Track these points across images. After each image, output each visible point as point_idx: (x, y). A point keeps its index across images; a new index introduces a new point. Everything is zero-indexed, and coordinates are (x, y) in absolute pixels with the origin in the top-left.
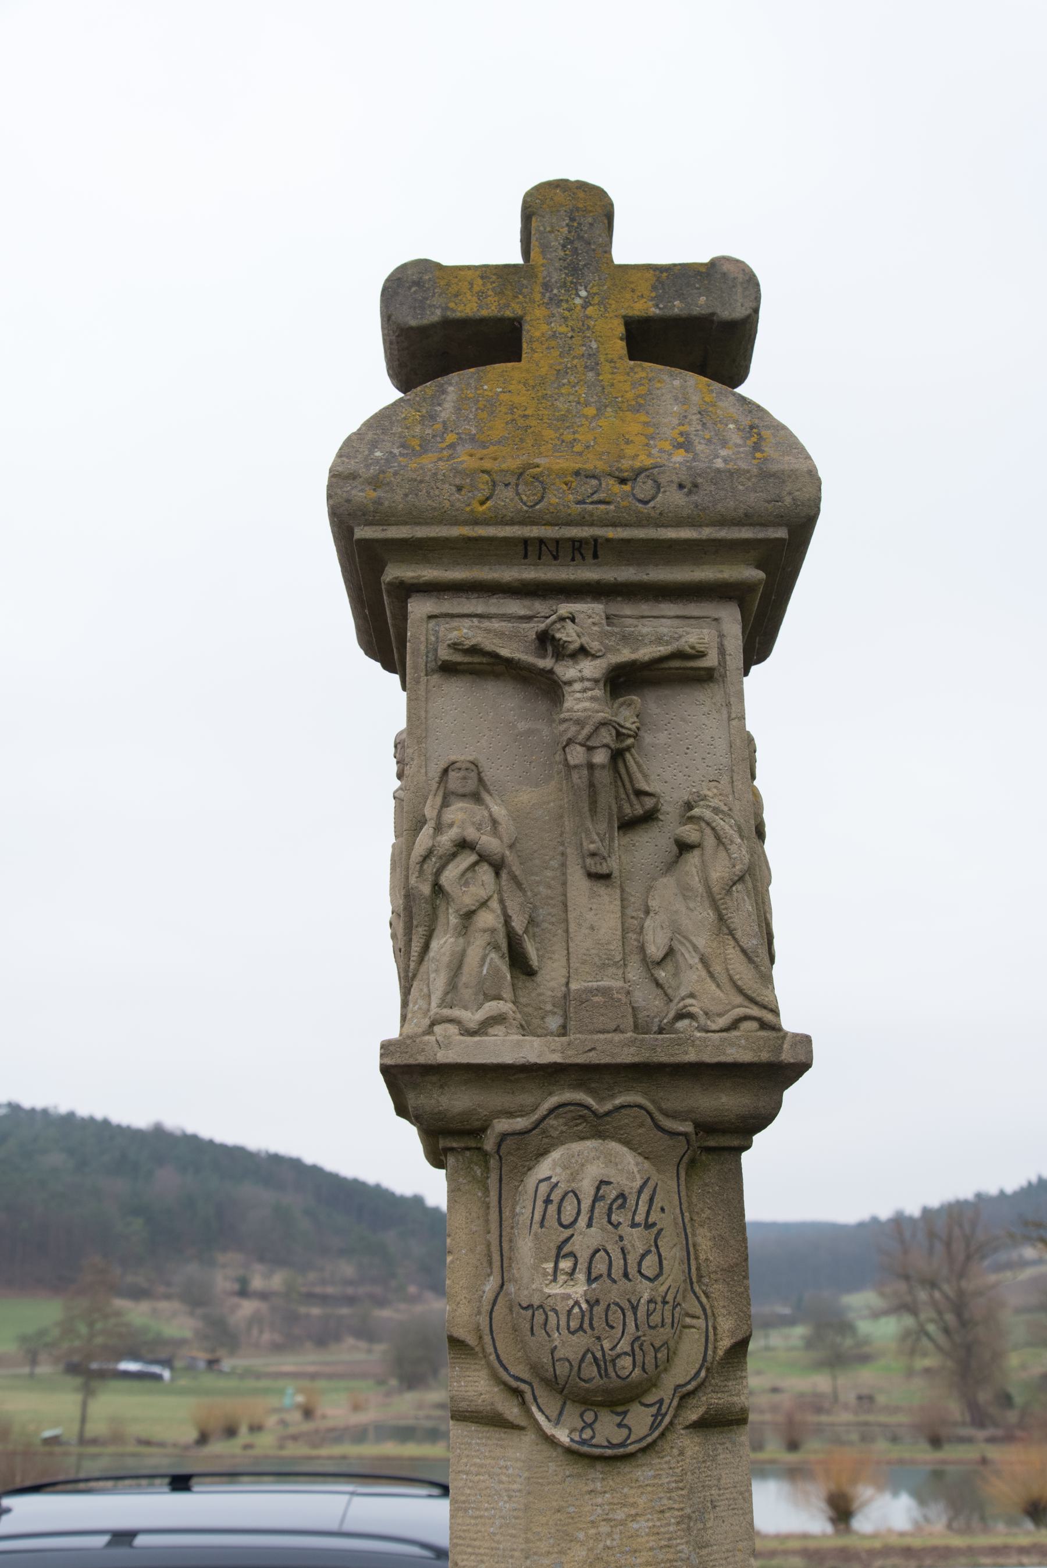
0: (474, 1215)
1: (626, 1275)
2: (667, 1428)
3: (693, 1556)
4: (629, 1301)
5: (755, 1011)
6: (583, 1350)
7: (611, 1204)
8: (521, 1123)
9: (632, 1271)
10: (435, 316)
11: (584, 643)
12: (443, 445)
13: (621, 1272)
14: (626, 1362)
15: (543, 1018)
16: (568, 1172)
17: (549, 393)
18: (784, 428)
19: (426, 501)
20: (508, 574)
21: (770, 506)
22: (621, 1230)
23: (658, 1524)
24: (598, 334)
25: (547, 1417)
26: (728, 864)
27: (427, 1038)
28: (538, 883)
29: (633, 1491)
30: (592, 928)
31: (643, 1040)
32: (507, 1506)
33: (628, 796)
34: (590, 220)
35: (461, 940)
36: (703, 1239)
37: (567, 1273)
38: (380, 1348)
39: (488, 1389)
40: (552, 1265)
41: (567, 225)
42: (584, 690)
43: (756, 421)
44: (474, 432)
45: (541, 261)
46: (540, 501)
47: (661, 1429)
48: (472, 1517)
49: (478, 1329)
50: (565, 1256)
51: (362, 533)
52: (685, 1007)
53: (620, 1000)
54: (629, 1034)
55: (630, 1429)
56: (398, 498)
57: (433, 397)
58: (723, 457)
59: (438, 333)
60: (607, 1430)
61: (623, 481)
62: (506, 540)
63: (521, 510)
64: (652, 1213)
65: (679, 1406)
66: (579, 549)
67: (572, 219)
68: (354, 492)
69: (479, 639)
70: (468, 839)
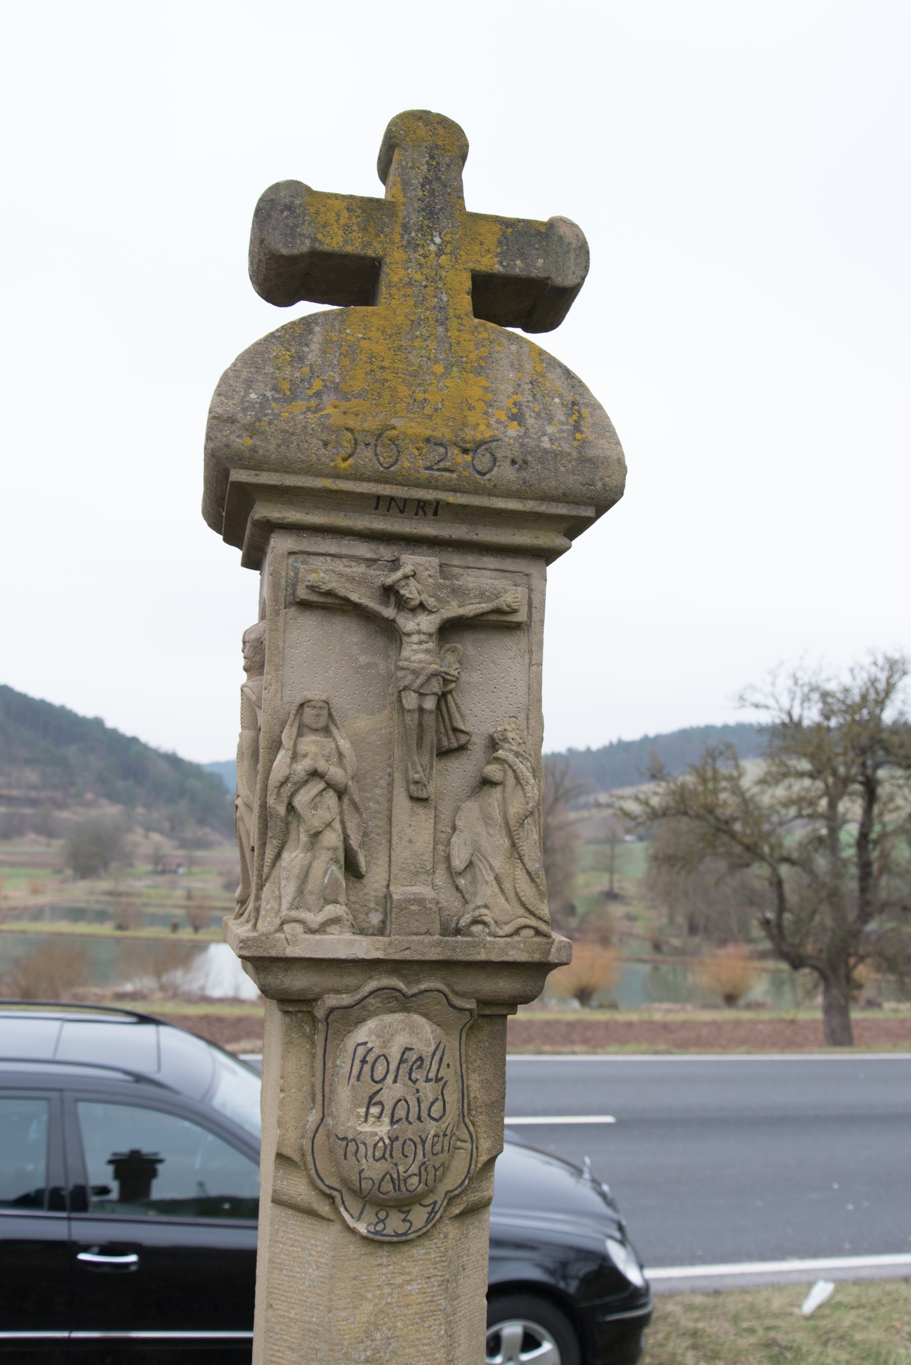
0: (303, 1062)
1: (419, 1118)
2: (438, 1220)
3: (449, 1306)
4: (420, 1137)
5: (533, 922)
6: (384, 1173)
7: (412, 1065)
8: (346, 999)
9: (424, 1115)
10: (304, 247)
11: (423, 600)
12: (310, 392)
13: (416, 1116)
14: (415, 1180)
15: (367, 914)
16: (381, 1040)
17: (404, 344)
18: (600, 407)
19: (296, 453)
20: (361, 522)
21: (584, 489)
22: (418, 1085)
23: (425, 1286)
24: (449, 286)
25: (351, 1215)
26: (523, 802)
27: (278, 935)
28: (369, 799)
29: (409, 1264)
30: (411, 842)
31: (447, 942)
32: (316, 1273)
33: (446, 731)
34: (447, 160)
35: (309, 855)
36: (474, 1083)
37: (375, 1117)
38: (58, 844)
39: (307, 1192)
40: (364, 1110)
41: (427, 163)
42: (421, 643)
43: (578, 397)
44: (337, 380)
45: (403, 200)
46: (395, 463)
47: (433, 1222)
48: (285, 1275)
49: (301, 1148)
50: (375, 1104)
51: (238, 475)
52: (481, 915)
53: (431, 909)
54: (437, 937)
55: (411, 1223)
56: (272, 448)
57: (301, 335)
58: (549, 435)
59: (305, 255)
60: (395, 1223)
61: (465, 451)
62: (362, 495)
63: (377, 471)
64: (441, 1070)
65: (448, 1204)
66: (423, 508)
67: (432, 157)
68: (232, 437)
69: (334, 584)
70: (319, 770)
